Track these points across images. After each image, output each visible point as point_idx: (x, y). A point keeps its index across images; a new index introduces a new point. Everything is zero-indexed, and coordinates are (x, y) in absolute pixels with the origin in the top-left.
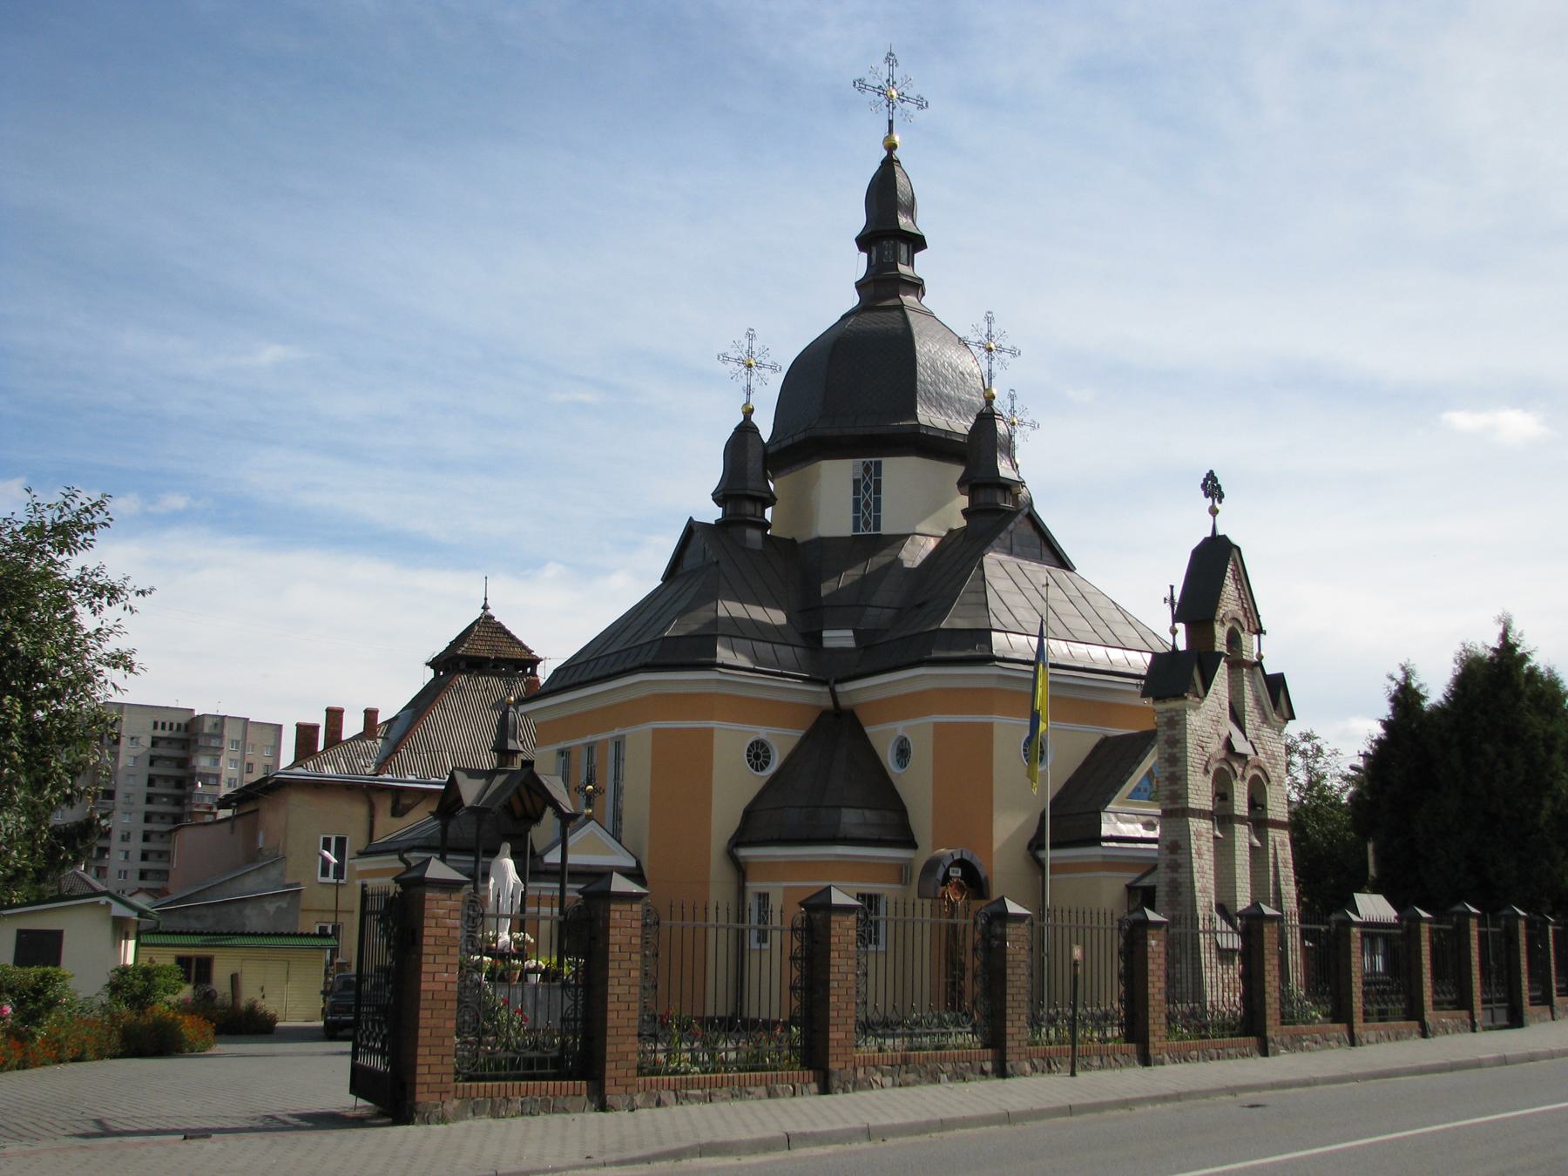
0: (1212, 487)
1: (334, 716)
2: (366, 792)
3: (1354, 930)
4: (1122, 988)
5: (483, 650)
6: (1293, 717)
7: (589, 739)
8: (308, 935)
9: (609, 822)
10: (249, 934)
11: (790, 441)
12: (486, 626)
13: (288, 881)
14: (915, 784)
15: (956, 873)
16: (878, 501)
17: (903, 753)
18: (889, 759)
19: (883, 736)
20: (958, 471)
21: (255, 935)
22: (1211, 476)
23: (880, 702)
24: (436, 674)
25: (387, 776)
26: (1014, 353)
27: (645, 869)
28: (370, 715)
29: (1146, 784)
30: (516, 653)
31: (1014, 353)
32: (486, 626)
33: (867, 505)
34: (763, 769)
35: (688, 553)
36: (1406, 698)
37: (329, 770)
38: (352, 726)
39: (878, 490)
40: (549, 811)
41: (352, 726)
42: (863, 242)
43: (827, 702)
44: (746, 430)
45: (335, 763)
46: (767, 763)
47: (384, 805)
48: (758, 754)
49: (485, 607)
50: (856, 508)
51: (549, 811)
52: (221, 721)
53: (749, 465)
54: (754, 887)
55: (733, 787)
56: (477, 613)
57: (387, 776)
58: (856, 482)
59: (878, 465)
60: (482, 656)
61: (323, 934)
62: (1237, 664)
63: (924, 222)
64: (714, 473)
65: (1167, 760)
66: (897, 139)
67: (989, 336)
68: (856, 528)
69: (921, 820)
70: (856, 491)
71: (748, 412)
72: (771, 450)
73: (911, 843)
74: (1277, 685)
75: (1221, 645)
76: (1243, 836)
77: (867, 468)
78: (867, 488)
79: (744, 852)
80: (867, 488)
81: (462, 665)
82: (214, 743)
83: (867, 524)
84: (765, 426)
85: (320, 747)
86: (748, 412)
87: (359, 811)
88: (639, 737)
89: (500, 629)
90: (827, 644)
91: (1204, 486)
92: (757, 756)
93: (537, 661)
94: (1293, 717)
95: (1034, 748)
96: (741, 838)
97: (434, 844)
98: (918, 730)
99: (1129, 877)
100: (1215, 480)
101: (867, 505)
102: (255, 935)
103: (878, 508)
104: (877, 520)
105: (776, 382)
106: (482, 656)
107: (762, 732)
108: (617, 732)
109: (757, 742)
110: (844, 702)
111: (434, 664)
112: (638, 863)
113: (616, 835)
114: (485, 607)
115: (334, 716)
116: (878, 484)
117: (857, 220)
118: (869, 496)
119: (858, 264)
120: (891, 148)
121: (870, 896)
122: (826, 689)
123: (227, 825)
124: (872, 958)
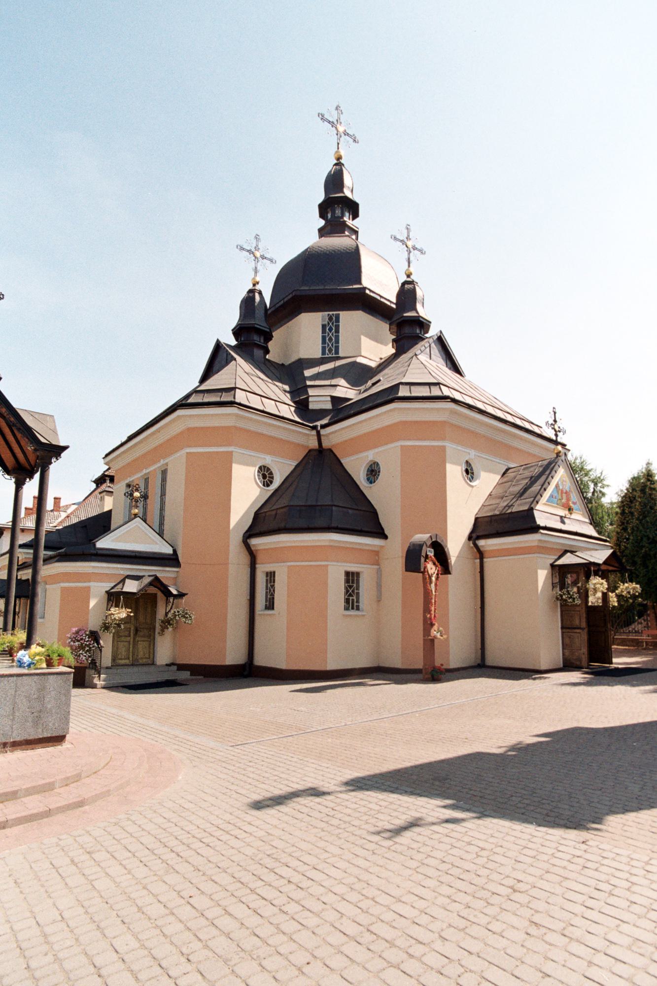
7: (145, 471)
9: (156, 526)
14: (384, 496)
15: (431, 553)
16: (337, 338)
17: (373, 472)
18: (360, 477)
19: (356, 466)
23: (360, 437)
27: (180, 553)
29: (555, 494)
33: (330, 339)
39: (337, 331)
43: (313, 444)
46: (271, 482)
50: (324, 341)
54: (262, 569)
55: (245, 493)
58: (324, 326)
64: (233, 318)
66: (342, 153)
69: (389, 519)
70: (324, 331)
77: (330, 318)
78: (330, 329)
80: (330, 329)
83: (330, 350)
84: (267, 291)
88: (177, 464)
90: (311, 407)
96: (252, 532)
97: (650, 667)
99: (107, 586)
101: (330, 339)
104: (337, 348)
107: (268, 460)
108: (162, 462)
110: (326, 444)
112: (175, 551)
113: (161, 534)
116: (337, 327)
117: (320, 196)
118: (332, 335)
120: (339, 158)
121: (353, 573)
122: (314, 432)
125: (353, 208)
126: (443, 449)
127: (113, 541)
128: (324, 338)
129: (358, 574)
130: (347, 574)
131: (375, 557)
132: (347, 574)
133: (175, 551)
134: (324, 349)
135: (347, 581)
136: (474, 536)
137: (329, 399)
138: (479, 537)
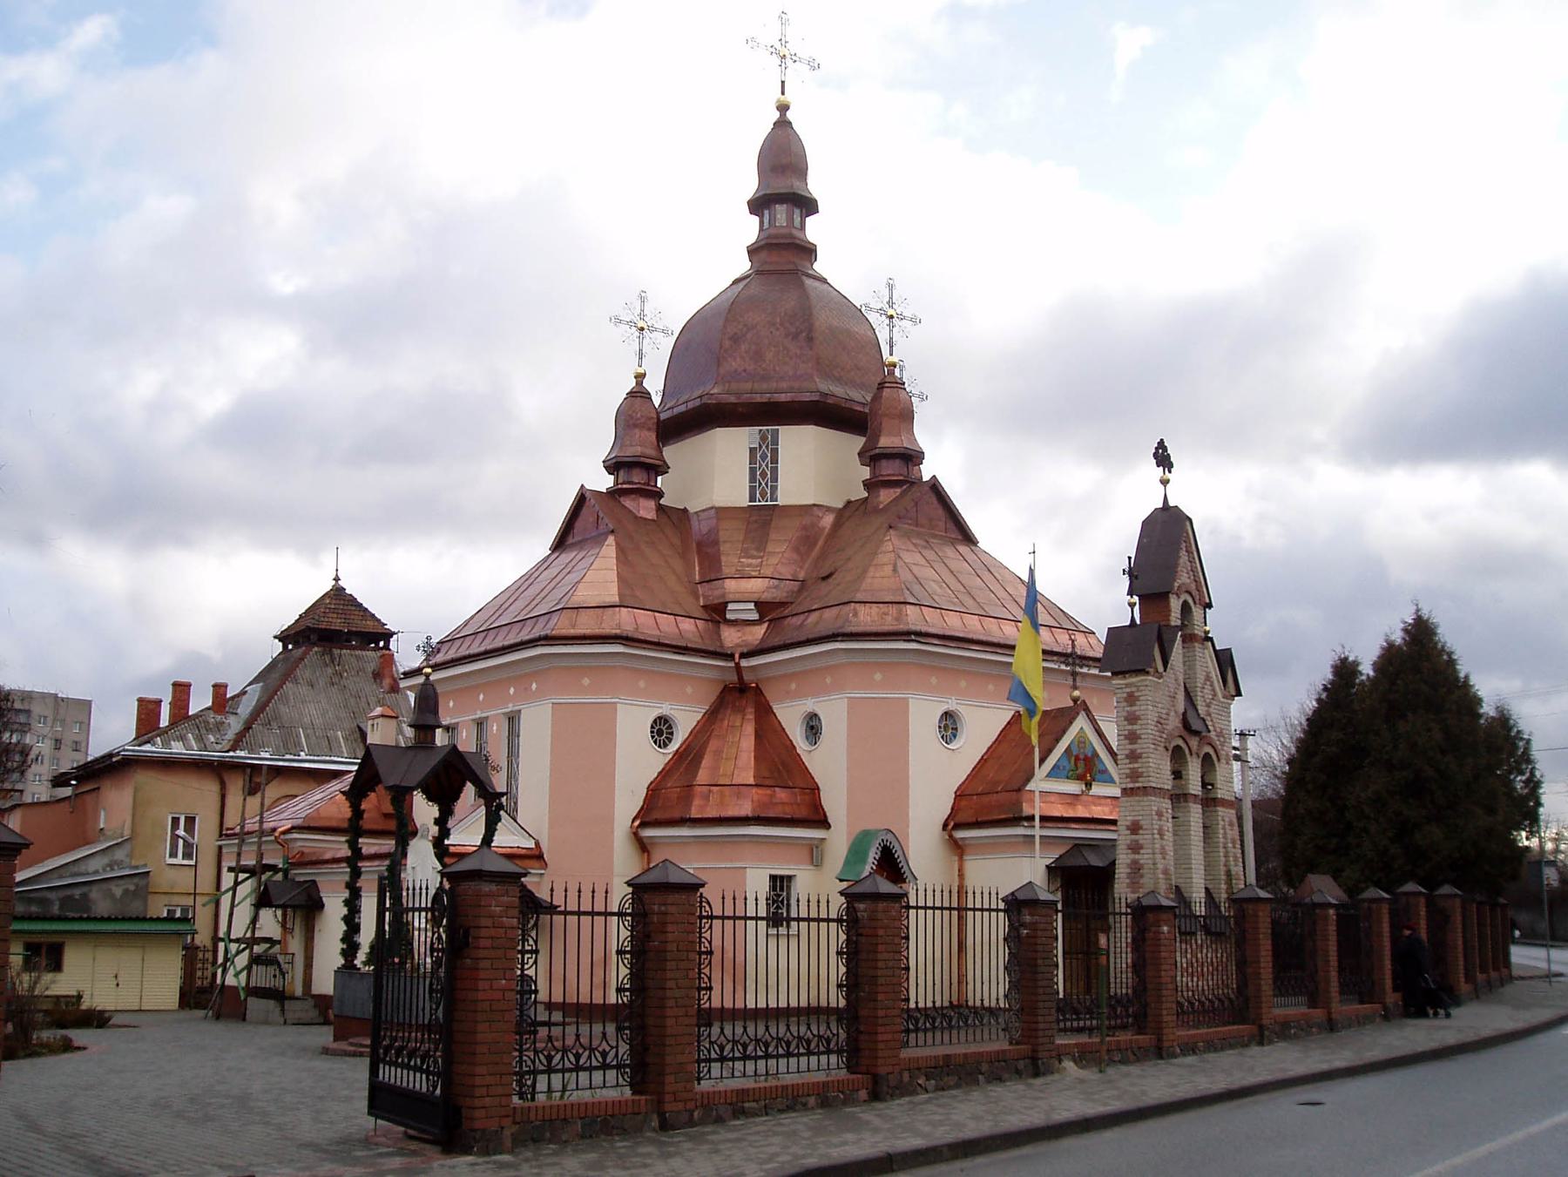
0: (1163, 459)
1: (181, 691)
2: (219, 770)
3: (1331, 912)
4: (843, 969)
5: (337, 624)
6: (1239, 694)
8: (159, 919)
10: (95, 919)
11: (682, 408)
12: (338, 597)
13: (134, 863)
16: (775, 471)
17: (813, 727)
20: (859, 442)
21: (102, 919)
22: (1161, 444)
24: (285, 647)
25: (242, 754)
26: (915, 321)
28: (219, 689)
29: (1065, 763)
30: (369, 626)
31: (915, 321)
32: (338, 597)
33: (763, 475)
34: (666, 745)
35: (941, 512)
36: (1345, 670)
37: (177, 748)
38: (200, 702)
39: (775, 460)
40: (469, 790)
41: (200, 702)
42: (758, 206)
44: (639, 394)
45: (182, 738)
47: (236, 787)
48: (662, 729)
49: (337, 579)
50: (753, 478)
51: (469, 790)
52: (27, 696)
53: (655, 431)
56: (328, 586)
57: (242, 754)
59: (776, 434)
60: (335, 632)
61: (170, 918)
62: (1189, 639)
63: (816, 185)
64: (603, 441)
65: (1127, 737)
67: (891, 304)
68: (752, 498)
69: (834, 802)
70: (752, 460)
71: (640, 377)
72: (663, 416)
73: (823, 822)
74: (1225, 661)
75: (1175, 619)
76: (1195, 812)
77: (763, 438)
78: (764, 457)
79: (648, 833)
80: (764, 457)
81: (313, 637)
82: (22, 718)
83: (763, 495)
85: (164, 721)
86: (640, 377)
87: (210, 788)
89: (352, 601)
91: (1155, 455)
92: (660, 733)
93: (388, 635)
94: (1239, 694)
95: (949, 725)
98: (834, 711)
100: (1165, 449)
101: (763, 475)
102: (102, 919)
103: (775, 479)
104: (774, 489)
105: (668, 344)
106: (335, 632)
107: (665, 709)
109: (660, 718)
111: (284, 637)
112: (537, 844)
114: (337, 579)
115: (181, 691)
116: (775, 452)
117: (749, 184)
118: (766, 466)
119: (749, 229)
121: (782, 878)
123: (65, 806)
124: (783, 942)
125: (808, 206)
126: (906, 699)
127: (1042, 761)
128: (752, 471)
129: (790, 878)
130: (773, 878)
131: (815, 853)
132: (773, 878)
133: (537, 844)
134: (752, 490)
135: (773, 888)
136: (953, 823)
137: (752, 606)
138: (957, 826)
